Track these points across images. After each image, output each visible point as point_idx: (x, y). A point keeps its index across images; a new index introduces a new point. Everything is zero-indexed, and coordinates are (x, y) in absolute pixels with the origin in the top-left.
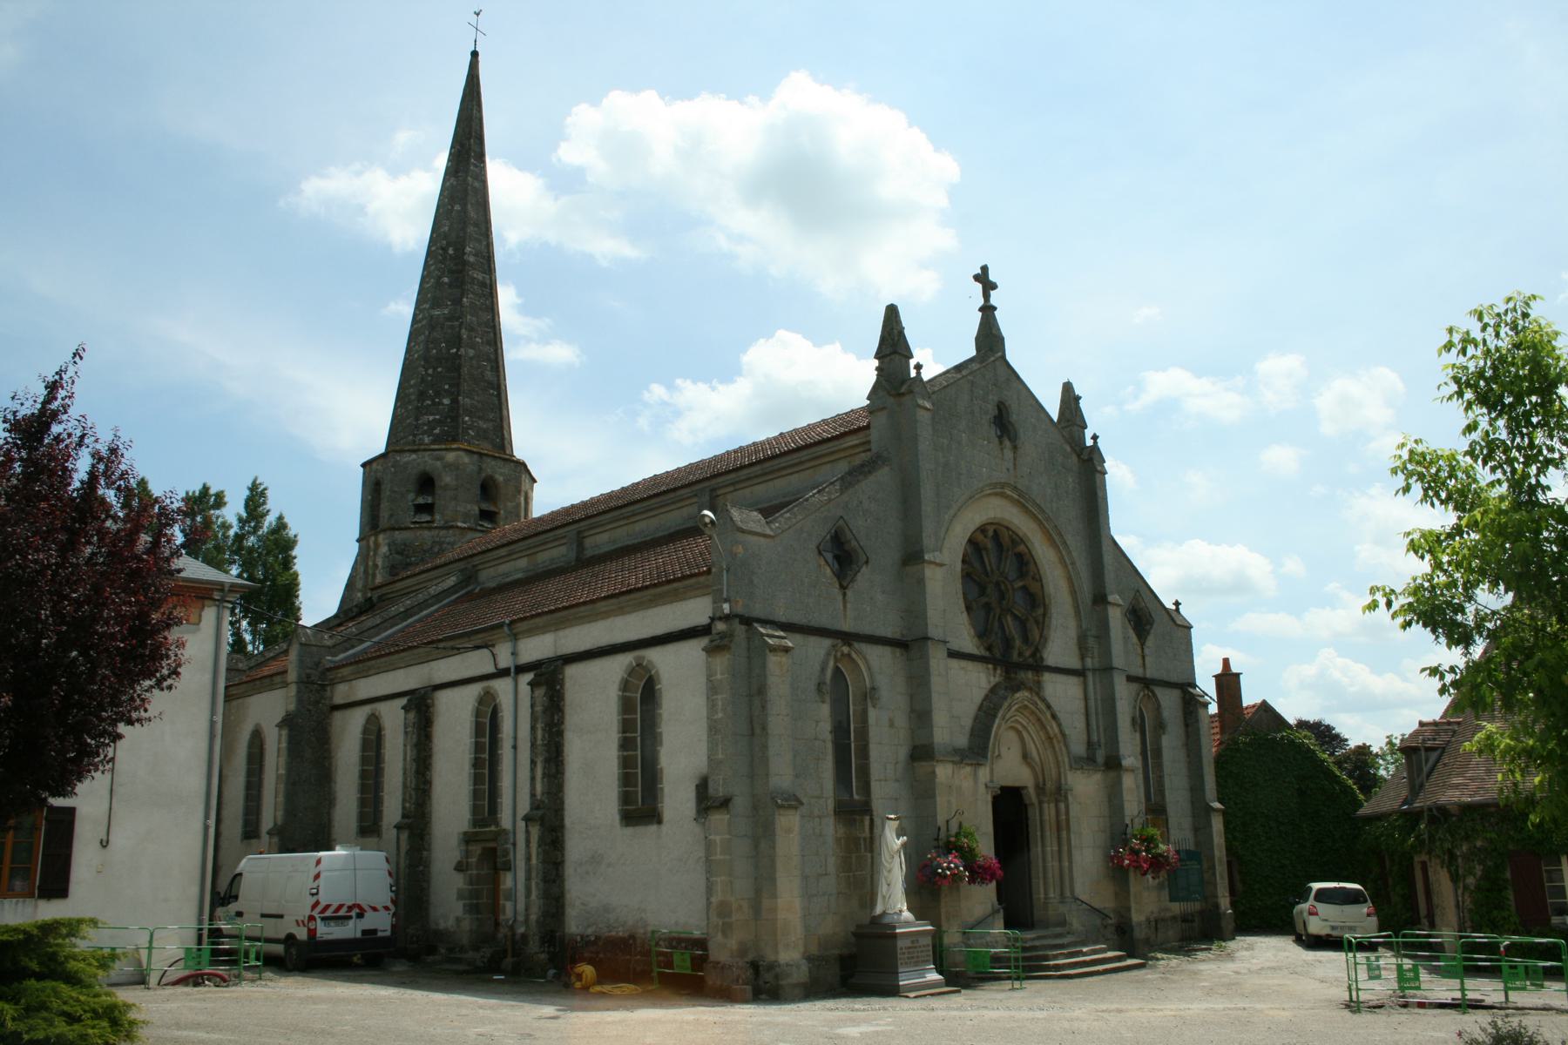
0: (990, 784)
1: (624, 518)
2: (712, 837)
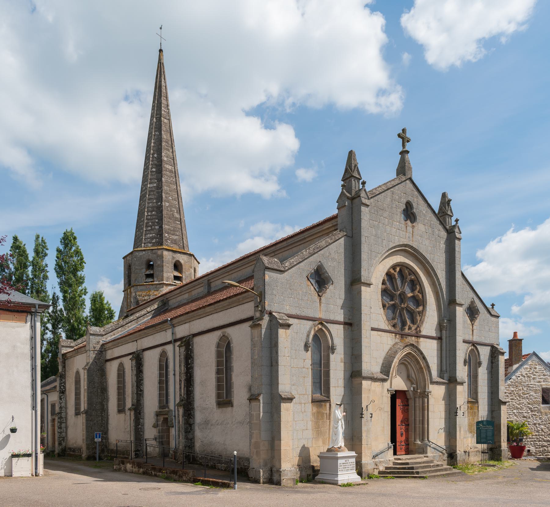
0: (390, 389)
1: (227, 272)
2: (252, 413)
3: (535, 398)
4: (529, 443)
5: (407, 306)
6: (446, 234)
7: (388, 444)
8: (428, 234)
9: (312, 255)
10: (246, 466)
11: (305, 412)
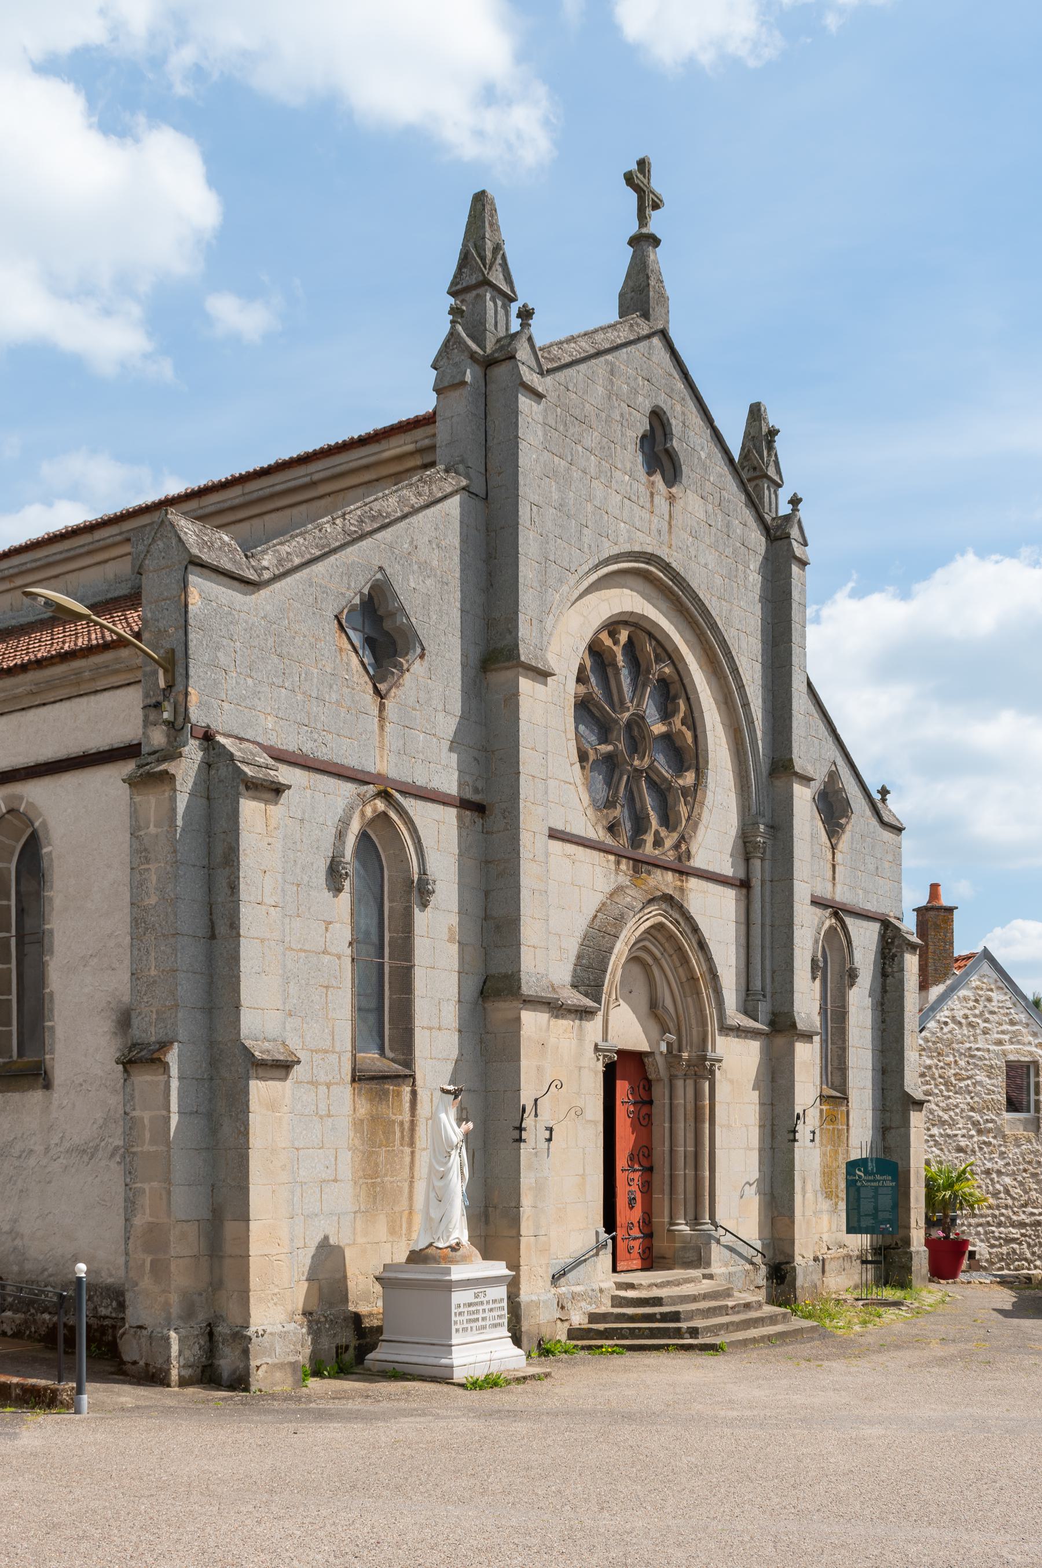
0: (602, 1045)
2: (135, 1114)
3: (990, 1092)
4: (973, 1232)
5: (651, 767)
6: (764, 539)
7: (597, 1233)
8: (713, 530)
9: (354, 541)
10: (105, 1317)
11: (329, 1116)
